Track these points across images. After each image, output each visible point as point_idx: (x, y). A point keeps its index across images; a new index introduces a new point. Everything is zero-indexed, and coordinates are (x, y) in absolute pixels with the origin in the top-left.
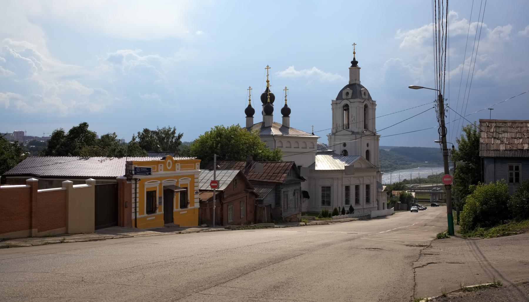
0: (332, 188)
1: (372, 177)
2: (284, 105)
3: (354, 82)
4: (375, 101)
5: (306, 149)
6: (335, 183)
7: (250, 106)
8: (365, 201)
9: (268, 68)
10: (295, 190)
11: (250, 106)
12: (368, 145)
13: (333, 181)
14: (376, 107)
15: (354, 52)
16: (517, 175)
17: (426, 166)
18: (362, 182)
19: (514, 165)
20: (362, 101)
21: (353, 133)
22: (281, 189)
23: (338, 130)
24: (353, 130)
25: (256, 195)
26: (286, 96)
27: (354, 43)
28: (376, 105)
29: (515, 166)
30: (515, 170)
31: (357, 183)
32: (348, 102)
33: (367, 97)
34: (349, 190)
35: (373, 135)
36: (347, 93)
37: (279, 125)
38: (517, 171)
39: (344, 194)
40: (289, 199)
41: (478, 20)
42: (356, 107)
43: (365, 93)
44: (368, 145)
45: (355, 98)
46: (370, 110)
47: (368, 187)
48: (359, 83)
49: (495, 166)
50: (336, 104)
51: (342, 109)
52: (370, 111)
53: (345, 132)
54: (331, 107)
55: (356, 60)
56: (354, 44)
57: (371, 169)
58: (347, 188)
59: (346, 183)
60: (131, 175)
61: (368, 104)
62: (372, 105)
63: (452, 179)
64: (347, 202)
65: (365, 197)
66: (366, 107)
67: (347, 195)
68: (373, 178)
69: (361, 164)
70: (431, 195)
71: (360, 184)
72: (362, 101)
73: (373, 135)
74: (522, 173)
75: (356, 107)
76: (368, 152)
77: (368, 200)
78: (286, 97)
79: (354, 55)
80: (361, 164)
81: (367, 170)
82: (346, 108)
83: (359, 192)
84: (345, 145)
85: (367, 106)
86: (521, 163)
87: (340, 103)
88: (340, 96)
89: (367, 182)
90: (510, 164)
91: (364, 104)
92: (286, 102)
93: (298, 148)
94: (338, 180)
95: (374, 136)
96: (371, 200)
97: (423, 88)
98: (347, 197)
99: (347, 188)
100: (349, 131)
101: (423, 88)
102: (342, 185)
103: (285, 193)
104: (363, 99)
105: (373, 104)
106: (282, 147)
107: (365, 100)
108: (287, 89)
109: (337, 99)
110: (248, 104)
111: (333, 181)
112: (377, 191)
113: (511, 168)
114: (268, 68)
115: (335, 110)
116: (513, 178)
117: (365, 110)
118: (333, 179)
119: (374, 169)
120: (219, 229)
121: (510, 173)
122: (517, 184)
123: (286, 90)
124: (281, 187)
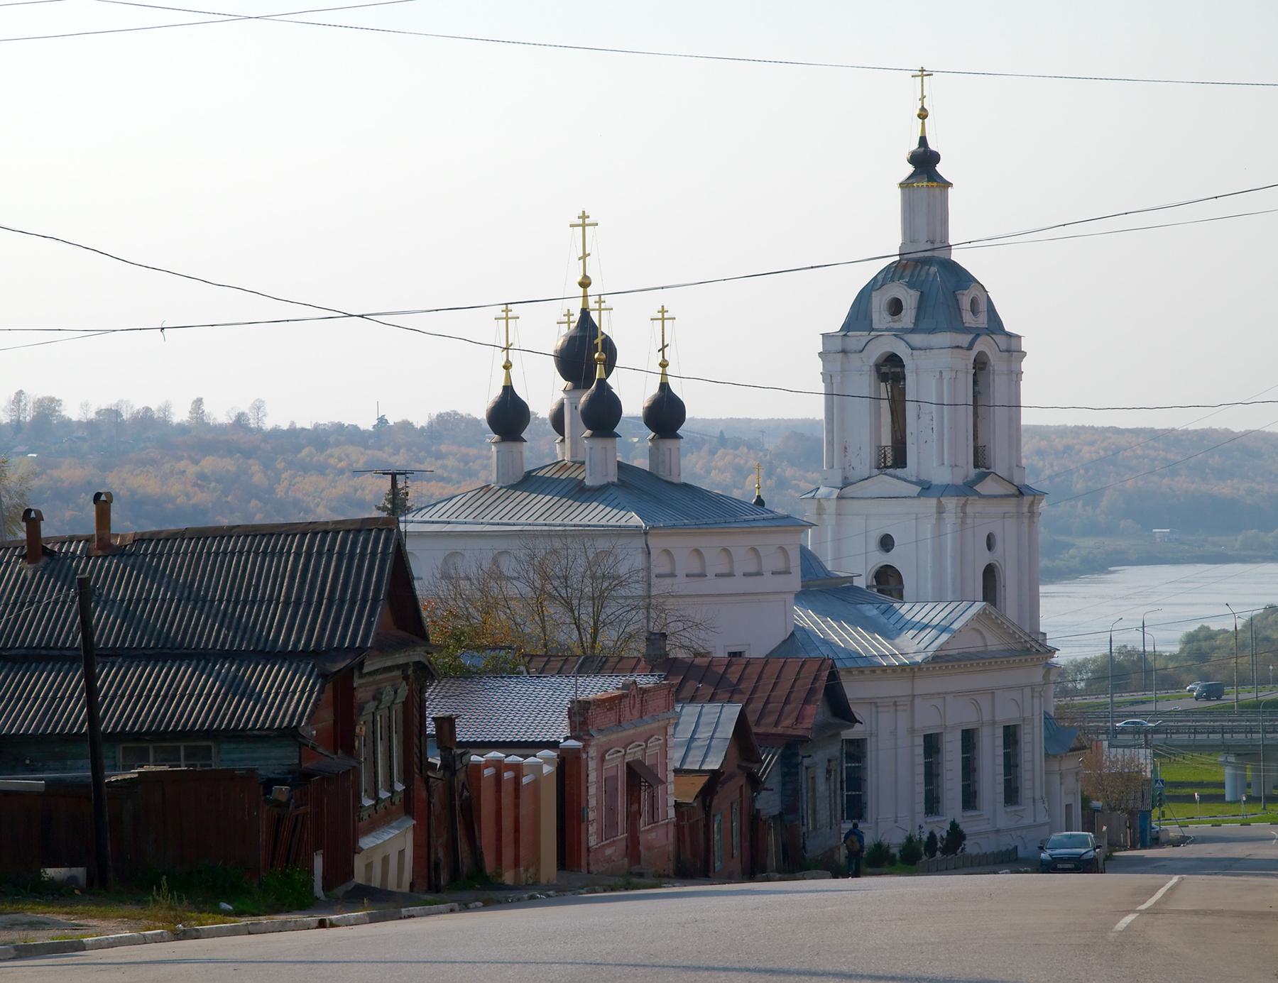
0: (870, 747)
1: (1028, 691)
2: (658, 385)
4: (1020, 337)
7: (508, 390)
8: (1001, 797)
9: (584, 222)
10: (829, 761)
11: (508, 390)
13: (877, 712)
14: (1025, 365)
15: (923, 109)
17: (722, 440)
21: (926, 488)
22: (803, 757)
24: (924, 477)
26: (664, 347)
28: (1025, 354)
31: (969, 718)
32: (901, 350)
33: (982, 321)
34: (974, 748)
36: (896, 307)
37: (1042, 596)
39: (921, 770)
40: (817, 794)
42: (941, 372)
45: (932, 331)
46: (996, 378)
48: (946, 257)
50: (844, 351)
51: (874, 374)
52: (998, 391)
53: (886, 484)
54: (818, 365)
55: (932, 146)
57: (1023, 658)
58: (932, 744)
59: (928, 721)
60: (586, 737)
66: (980, 365)
67: (932, 774)
68: (1033, 697)
69: (981, 633)
70: (1232, 759)
72: (965, 339)
75: (941, 372)
76: (990, 574)
77: (1011, 794)
78: (662, 350)
79: (923, 124)
80: (981, 633)
81: (1008, 662)
83: (1016, 755)
85: (985, 364)
87: (861, 351)
88: (859, 315)
89: (1007, 713)
91: (973, 353)
93: (731, 575)
94: (896, 711)
96: (1026, 793)
98: (932, 784)
99: (932, 744)
100: (905, 480)
102: (912, 731)
103: (810, 770)
104: (967, 330)
105: (1008, 351)
107: (978, 335)
108: (666, 315)
109: (847, 327)
110: (503, 384)
111: (877, 712)
112: (1045, 754)
114: (584, 226)
117: (975, 382)
118: (877, 707)
119: (1035, 657)
123: (663, 319)
124: (802, 752)
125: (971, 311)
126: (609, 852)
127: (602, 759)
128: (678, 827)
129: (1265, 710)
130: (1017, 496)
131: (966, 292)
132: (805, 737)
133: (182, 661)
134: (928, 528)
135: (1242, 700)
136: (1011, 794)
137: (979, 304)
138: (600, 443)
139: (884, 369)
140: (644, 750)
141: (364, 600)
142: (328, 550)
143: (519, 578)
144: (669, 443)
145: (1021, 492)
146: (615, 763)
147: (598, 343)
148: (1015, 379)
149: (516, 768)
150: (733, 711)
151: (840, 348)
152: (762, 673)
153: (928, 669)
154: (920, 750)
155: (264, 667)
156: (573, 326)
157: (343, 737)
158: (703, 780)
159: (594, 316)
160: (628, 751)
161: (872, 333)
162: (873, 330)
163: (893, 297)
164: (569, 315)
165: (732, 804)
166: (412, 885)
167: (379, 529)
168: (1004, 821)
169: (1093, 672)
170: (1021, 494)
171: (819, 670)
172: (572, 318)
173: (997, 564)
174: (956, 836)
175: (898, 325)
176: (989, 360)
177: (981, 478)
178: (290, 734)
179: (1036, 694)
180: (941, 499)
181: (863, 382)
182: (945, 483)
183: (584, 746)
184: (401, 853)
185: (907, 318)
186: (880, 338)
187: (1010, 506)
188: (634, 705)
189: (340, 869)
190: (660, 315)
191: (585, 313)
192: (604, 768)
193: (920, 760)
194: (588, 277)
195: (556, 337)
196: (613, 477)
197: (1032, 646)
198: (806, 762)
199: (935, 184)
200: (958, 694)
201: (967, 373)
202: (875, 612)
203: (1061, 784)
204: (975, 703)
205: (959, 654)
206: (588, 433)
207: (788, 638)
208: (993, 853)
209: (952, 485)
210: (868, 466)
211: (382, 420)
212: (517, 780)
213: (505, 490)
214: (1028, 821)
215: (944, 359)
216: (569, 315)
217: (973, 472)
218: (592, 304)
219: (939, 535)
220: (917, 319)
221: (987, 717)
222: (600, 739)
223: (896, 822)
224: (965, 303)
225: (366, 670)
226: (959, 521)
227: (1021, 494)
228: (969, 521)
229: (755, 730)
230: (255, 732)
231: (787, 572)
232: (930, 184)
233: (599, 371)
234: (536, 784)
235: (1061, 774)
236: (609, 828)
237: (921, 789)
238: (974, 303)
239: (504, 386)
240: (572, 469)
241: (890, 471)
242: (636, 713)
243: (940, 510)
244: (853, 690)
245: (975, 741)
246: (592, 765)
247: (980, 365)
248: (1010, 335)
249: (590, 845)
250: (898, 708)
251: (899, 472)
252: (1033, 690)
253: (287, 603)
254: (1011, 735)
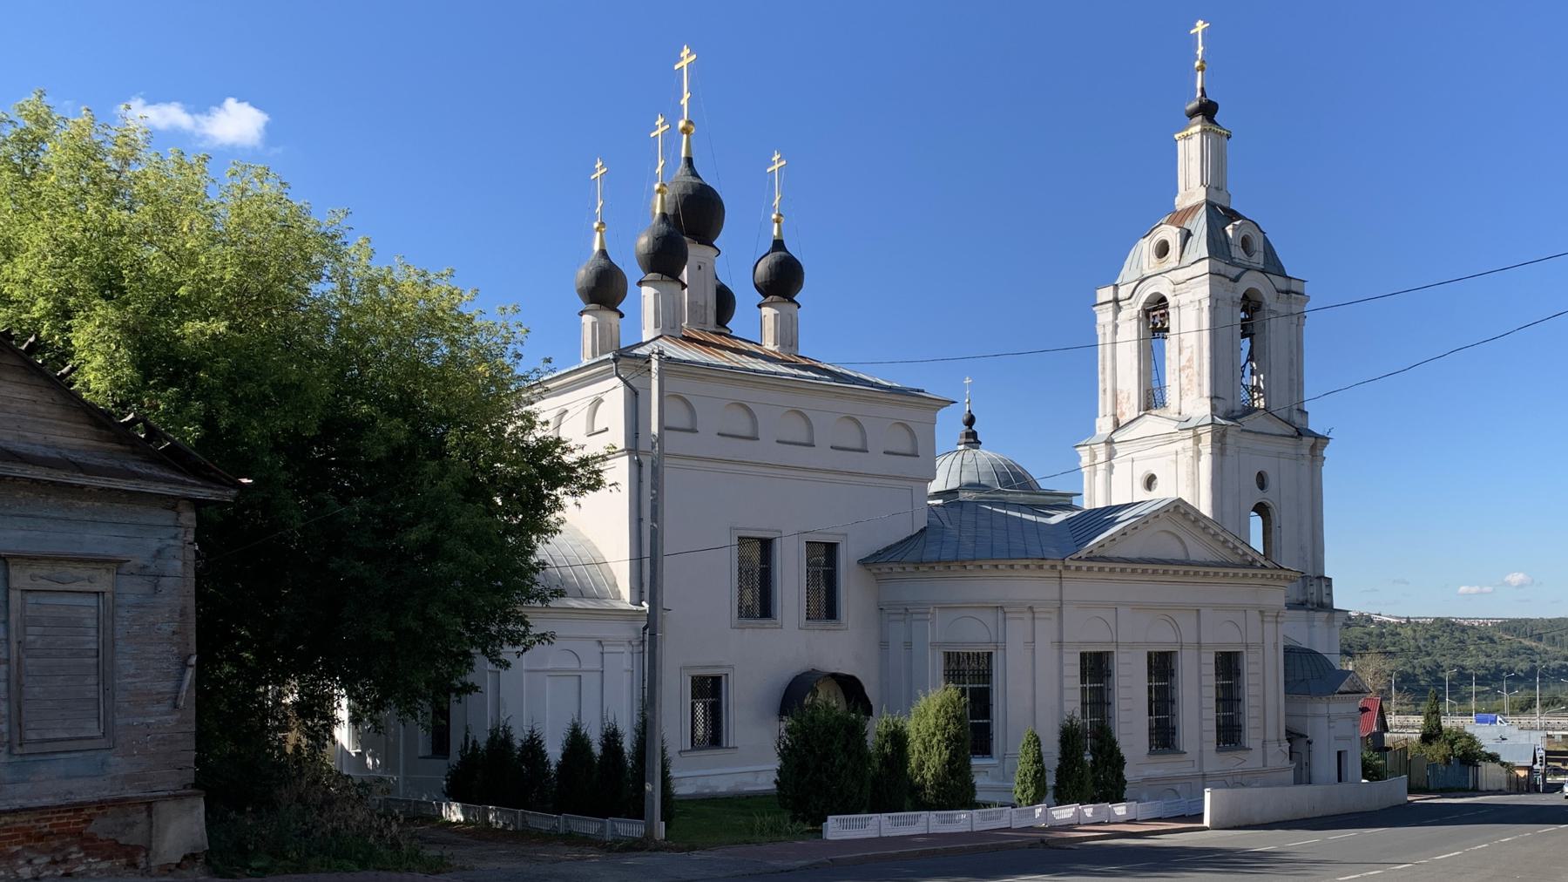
6: (1017, 630)
18: (1189, 637)
20: (1235, 271)
23: (1123, 421)
25: (18, 873)
31: (1163, 639)
41: (1301, 282)
43: (1246, 243)
44: (1261, 480)
47: (1228, 665)
58: (1096, 667)
61: (1262, 290)
65: (1211, 714)
72: (1235, 271)
96: (1251, 736)
99: (1096, 667)
104: (1237, 265)
120: (1100, 367)
125: (1243, 247)
129: (968, 692)
130: (1296, 438)
135: (171, 503)
137: (1252, 242)
145: (1301, 433)
163: (1164, 238)
169: (537, 440)
170: (1300, 434)
173: (1273, 506)
176: (1263, 298)
187: (1287, 446)
204: (1170, 621)
207: (916, 535)
213: (635, 351)
245: (1173, 667)
254: (1228, 665)
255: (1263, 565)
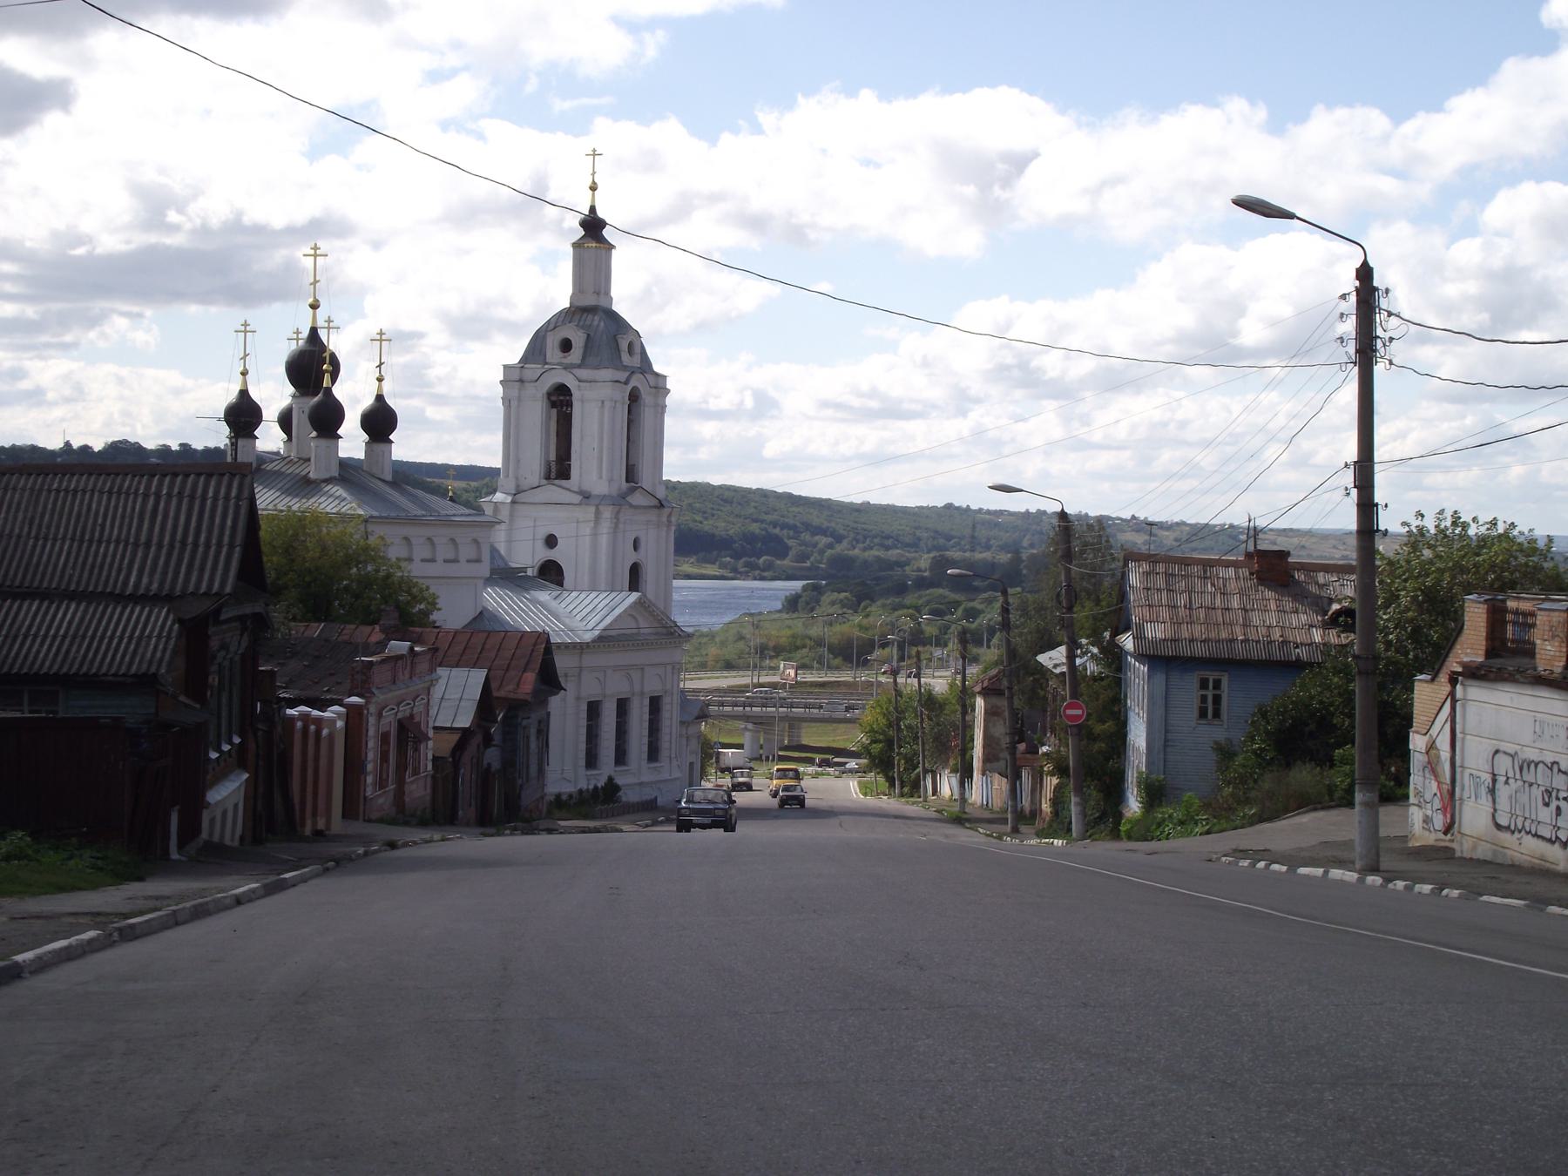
1: (669, 668)
3: (589, 301)
5: (477, 564)
8: (645, 756)
12: (636, 545)
15: (594, 182)
16: (1217, 700)
19: (1211, 676)
21: (586, 496)
24: (586, 487)
27: (594, 150)
28: (668, 391)
29: (1214, 680)
30: (1214, 688)
32: (570, 382)
35: (655, 507)
36: (566, 346)
38: (1218, 692)
42: (603, 402)
44: (636, 545)
45: (597, 368)
46: (646, 409)
49: (1167, 679)
50: (521, 381)
52: (647, 414)
53: (553, 492)
54: (499, 390)
55: (601, 214)
56: (594, 154)
59: (591, 690)
61: (641, 389)
62: (654, 390)
63: (1083, 712)
64: (592, 760)
65: (646, 740)
66: (634, 397)
70: (750, 726)
71: (633, 694)
72: (623, 376)
73: (655, 507)
74: (1229, 697)
75: (603, 402)
76: (635, 571)
77: (653, 753)
78: (379, 366)
79: (593, 195)
82: (560, 399)
83: (625, 723)
84: (551, 541)
86: (1226, 673)
90: (1202, 673)
91: (629, 388)
92: (380, 387)
93: (433, 560)
95: (656, 511)
96: (664, 754)
97: (1022, 491)
101: (1022, 491)
102: (578, 698)
104: (625, 368)
106: (410, 560)
107: (633, 372)
109: (525, 359)
113: (1204, 684)
115: (514, 404)
116: (1207, 707)
121: (1202, 695)
122: (1215, 723)
126: (381, 801)
127: (380, 715)
128: (433, 777)
131: (625, 336)
132: (526, 701)
133: (24, 600)
134: (587, 529)
136: (653, 753)
138: (323, 443)
139: (554, 398)
140: (412, 708)
141: (220, 545)
142: (179, 493)
143: (624, 498)
144: (381, 447)
146: (389, 718)
147: (325, 357)
148: (660, 411)
149: (319, 721)
150: (478, 677)
151: (518, 378)
152: (485, 643)
153: (594, 646)
154: (584, 715)
155: (115, 609)
156: (301, 342)
157: (195, 683)
158: (456, 737)
159: (323, 334)
160: (401, 709)
161: (546, 366)
162: (547, 363)
164: (298, 332)
165: (472, 759)
166: (242, 838)
167: (231, 474)
168: (647, 777)
171: (535, 645)
172: (300, 336)
174: (612, 789)
175: (567, 361)
177: (632, 490)
178: (146, 682)
179: (676, 671)
180: (601, 508)
181: (536, 412)
182: (603, 493)
183: (366, 703)
184: (236, 806)
185: (575, 355)
186: (553, 371)
187: (652, 516)
188: (406, 665)
189: (190, 829)
190: (378, 337)
191: (314, 331)
192: (381, 723)
193: (584, 722)
194: (318, 301)
195: (286, 348)
196: (335, 472)
197: (675, 631)
198: (525, 722)
199: (602, 245)
200: (616, 668)
201: (623, 404)
202: (548, 598)
203: (687, 745)
205: (619, 635)
206: (314, 434)
208: (638, 803)
209: (609, 496)
210: (538, 477)
211: (68, 444)
212: (318, 732)
214: (666, 776)
215: (606, 391)
216: (298, 332)
217: (625, 485)
218: (321, 323)
219: (595, 535)
220: (584, 358)
221: (637, 688)
222: (380, 697)
223: (562, 774)
224: (624, 345)
225: (223, 617)
226: (613, 525)
227: (661, 506)
228: (621, 526)
229: (495, 694)
230: (110, 678)
231: (478, 561)
232: (598, 245)
233: (326, 382)
234: (331, 736)
235: (687, 738)
236: (381, 783)
237: (583, 746)
238: (630, 346)
239: (240, 390)
240: (296, 466)
241: (557, 482)
242: (407, 676)
243: (598, 514)
244: (562, 662)
246: (372, 720)
247: (634, 397)
248: (657, 375)
249: (367, 795)
250: (569, 679)
251: (564, 483)
252: (673, 668)
253: (136, 545)
255: (680, 635)
